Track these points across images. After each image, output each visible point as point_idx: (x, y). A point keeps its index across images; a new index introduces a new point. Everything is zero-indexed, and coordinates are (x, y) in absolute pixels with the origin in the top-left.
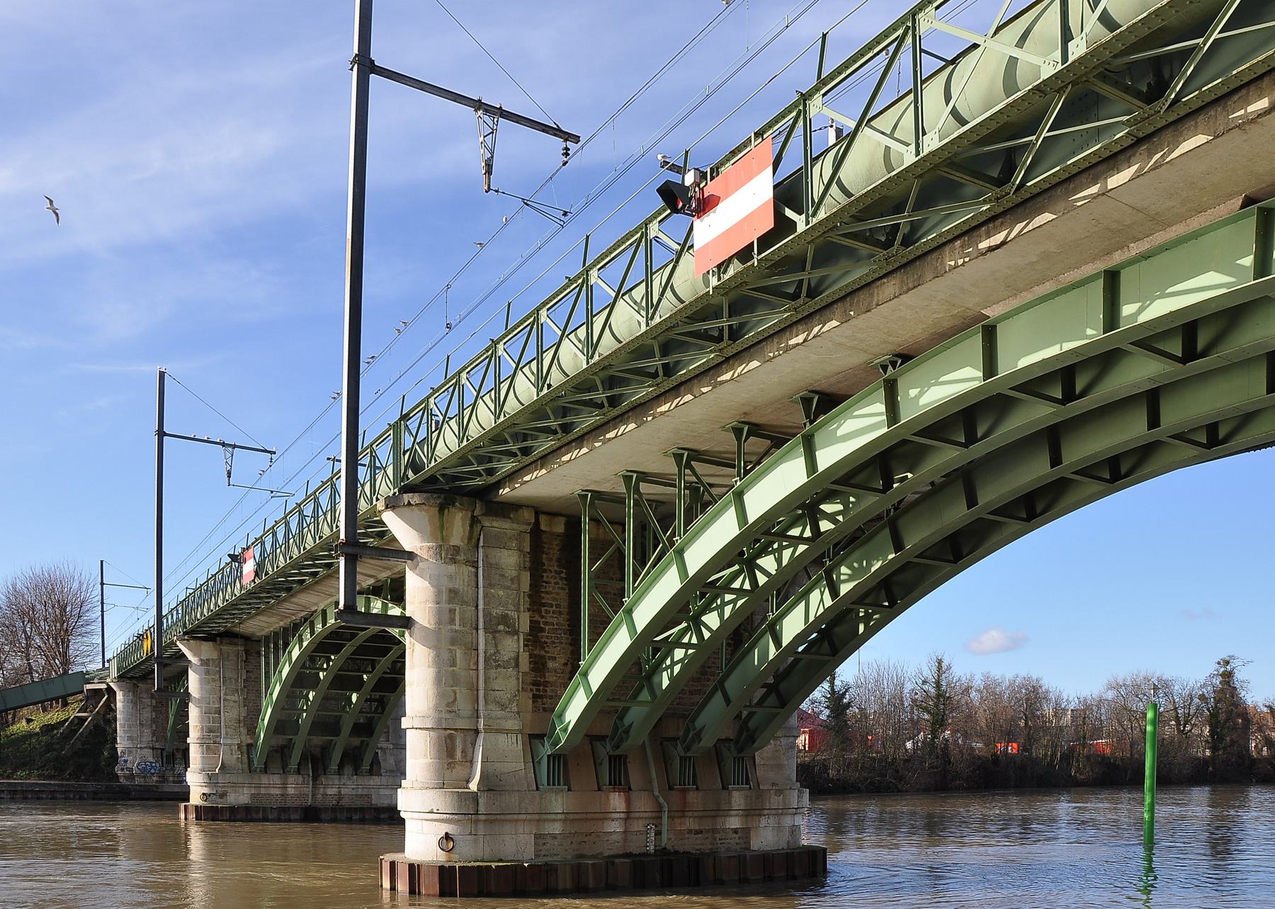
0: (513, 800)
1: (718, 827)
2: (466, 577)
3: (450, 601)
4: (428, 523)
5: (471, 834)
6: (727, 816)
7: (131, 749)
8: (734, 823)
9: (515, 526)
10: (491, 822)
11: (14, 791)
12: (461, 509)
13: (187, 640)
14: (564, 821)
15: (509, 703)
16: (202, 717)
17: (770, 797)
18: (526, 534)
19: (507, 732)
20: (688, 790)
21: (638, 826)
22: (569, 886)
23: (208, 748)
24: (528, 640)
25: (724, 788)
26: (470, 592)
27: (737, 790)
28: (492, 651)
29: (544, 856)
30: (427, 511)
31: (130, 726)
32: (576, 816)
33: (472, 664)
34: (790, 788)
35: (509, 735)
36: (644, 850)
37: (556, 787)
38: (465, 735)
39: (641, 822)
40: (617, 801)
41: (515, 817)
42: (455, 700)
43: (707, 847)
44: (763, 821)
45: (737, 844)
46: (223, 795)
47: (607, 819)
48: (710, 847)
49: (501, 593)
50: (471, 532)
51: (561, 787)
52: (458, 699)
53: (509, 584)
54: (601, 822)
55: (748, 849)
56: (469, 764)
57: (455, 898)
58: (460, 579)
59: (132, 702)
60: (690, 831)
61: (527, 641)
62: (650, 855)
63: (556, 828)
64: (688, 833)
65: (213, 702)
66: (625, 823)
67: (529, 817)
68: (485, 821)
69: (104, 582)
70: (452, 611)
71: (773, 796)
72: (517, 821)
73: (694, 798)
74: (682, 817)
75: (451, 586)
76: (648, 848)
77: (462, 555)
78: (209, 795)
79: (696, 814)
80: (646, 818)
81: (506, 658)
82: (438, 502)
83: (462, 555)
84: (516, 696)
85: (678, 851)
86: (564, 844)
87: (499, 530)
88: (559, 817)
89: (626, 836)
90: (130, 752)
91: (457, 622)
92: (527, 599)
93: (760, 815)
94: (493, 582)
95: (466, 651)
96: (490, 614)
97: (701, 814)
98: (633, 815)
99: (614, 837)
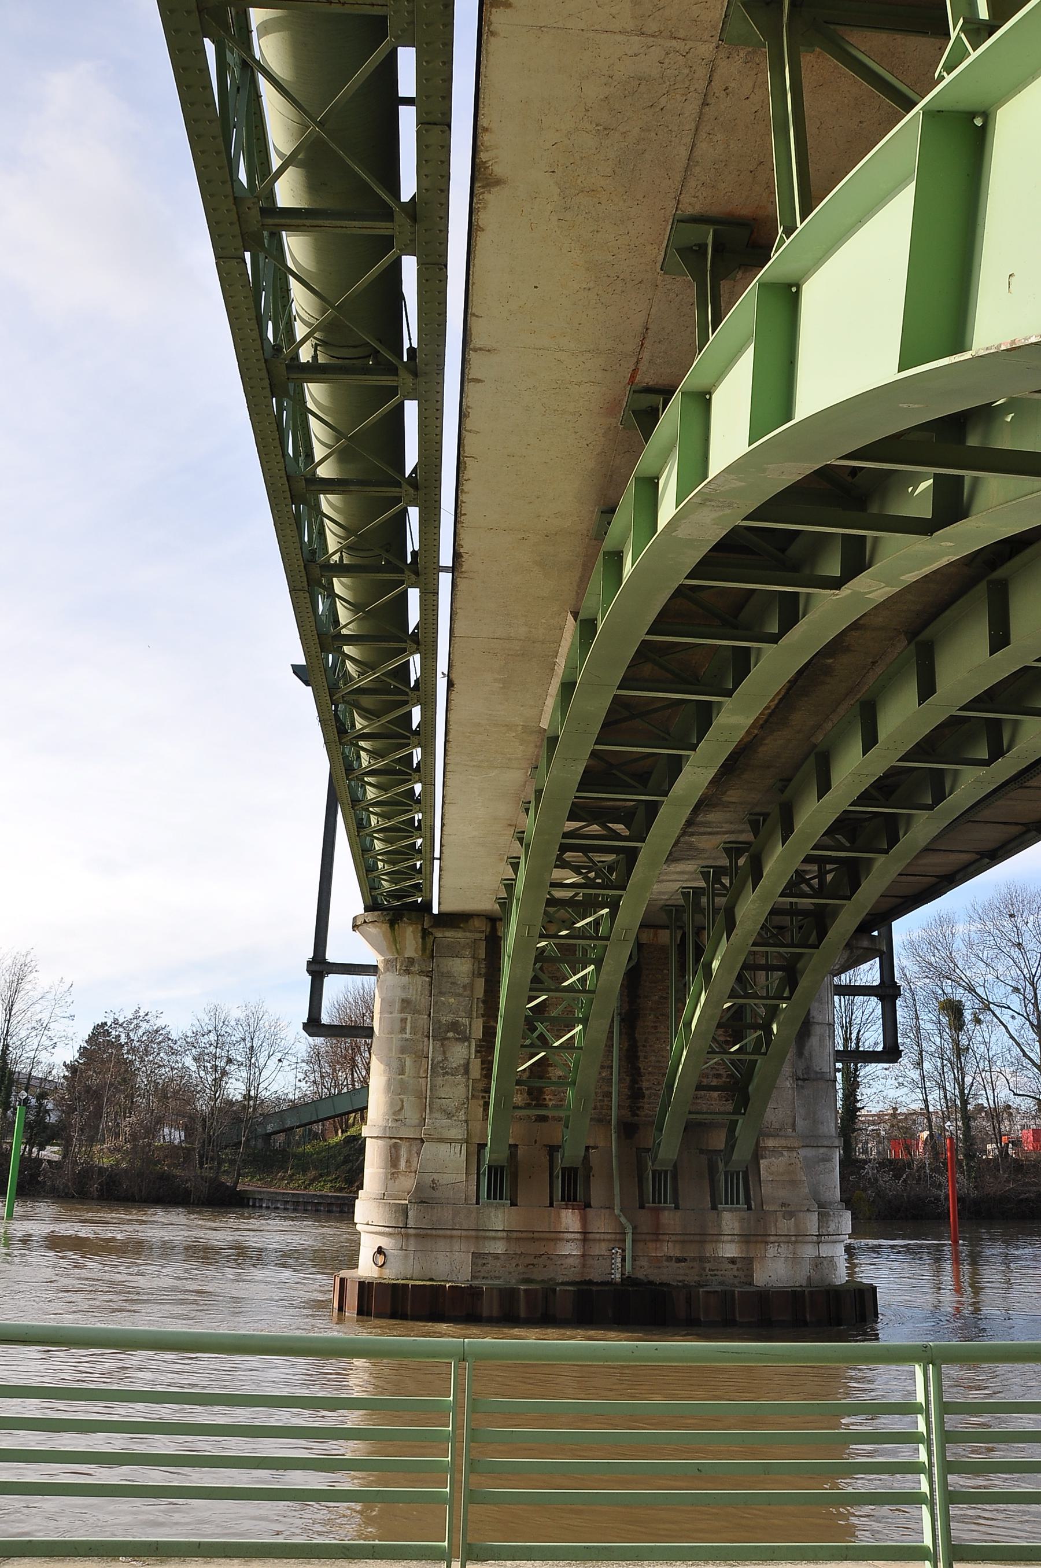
0: (446, 1214)
1: (708, 1255)
2: (420, 986)
3: (402, 1010)
4: (383, 939)
5: (401, 1249)
6: (717, 1241)
8: (730, 1250)
9: (468, 934)
10: (424, 1237)
11: (297, 1202)
12: (411, 924)
14: (508, 1239)
15: (457, 1111)
17: (777, 1221)
18: (482, 942)
19: (451, 1141)
20: (664, 1208)
21: (599, 1249)
22: (495, 1313)
24: (481, 1046)
25: (714, 1207)
26: (423, 1000)
27: (730, 1210)
28: (440, 1059)
29: (483, 1278)
30: (380, 928)
32: (519, 1235)
33: (421, 1071)
34: (808, 1210)
35: (453, 1144)
36: (607, 1278)
37: (498, 1201)
38: (411, 1145)
39: (604, 1246)
40: (570, 1220)
41: (448, 1232)
42: (402, 1108)
43: (692, 1278)
44: (771, 1251)
45: (735, 1277)
47: (561, 1240)
48: (697, 1278)
49: (452, 1000)
50: (424, 944)
51: (734, 1206)
52: (405, 1107)
53: (461, 991)
54: (553, 1243)
55: (751, 1284)
56: (413, 1174)
57: (369, 1318)
58: (413, 989)
60: (669, 1259)
61: (480, 1047)
62: (616, 1284)
63: (499, 1248)
64: (667, 1261)
66: (584, 1246)
67: (464, 1233)
68: (416, 1236)
69: (332, 956)
70: (404, 1020)
71: (780, 1219)
72: (452, 1237)
73: (670, 1219)
74: (657, 1241)
75: (404, 996)
76: (613, 1276)
77: (416, 966)
79: (673, 1238)
80: (609, 1240)
81: (454, 1065)
82: (387, 919)
83: (416, 966)
84: (464, 1104)
85: (653, 1282)
86: (508, 1265)
87: (452, 940)
88: (500, 1234)
89: (584, 1260)
91: (408, 1031)
92: (481, 1005)
93: (767, 1243)
94: (444, 990)
95: (416, 1059)
96: (439, 1022)
97: (679, 1238)
98: (591, 1236)
99: (570, 1261)
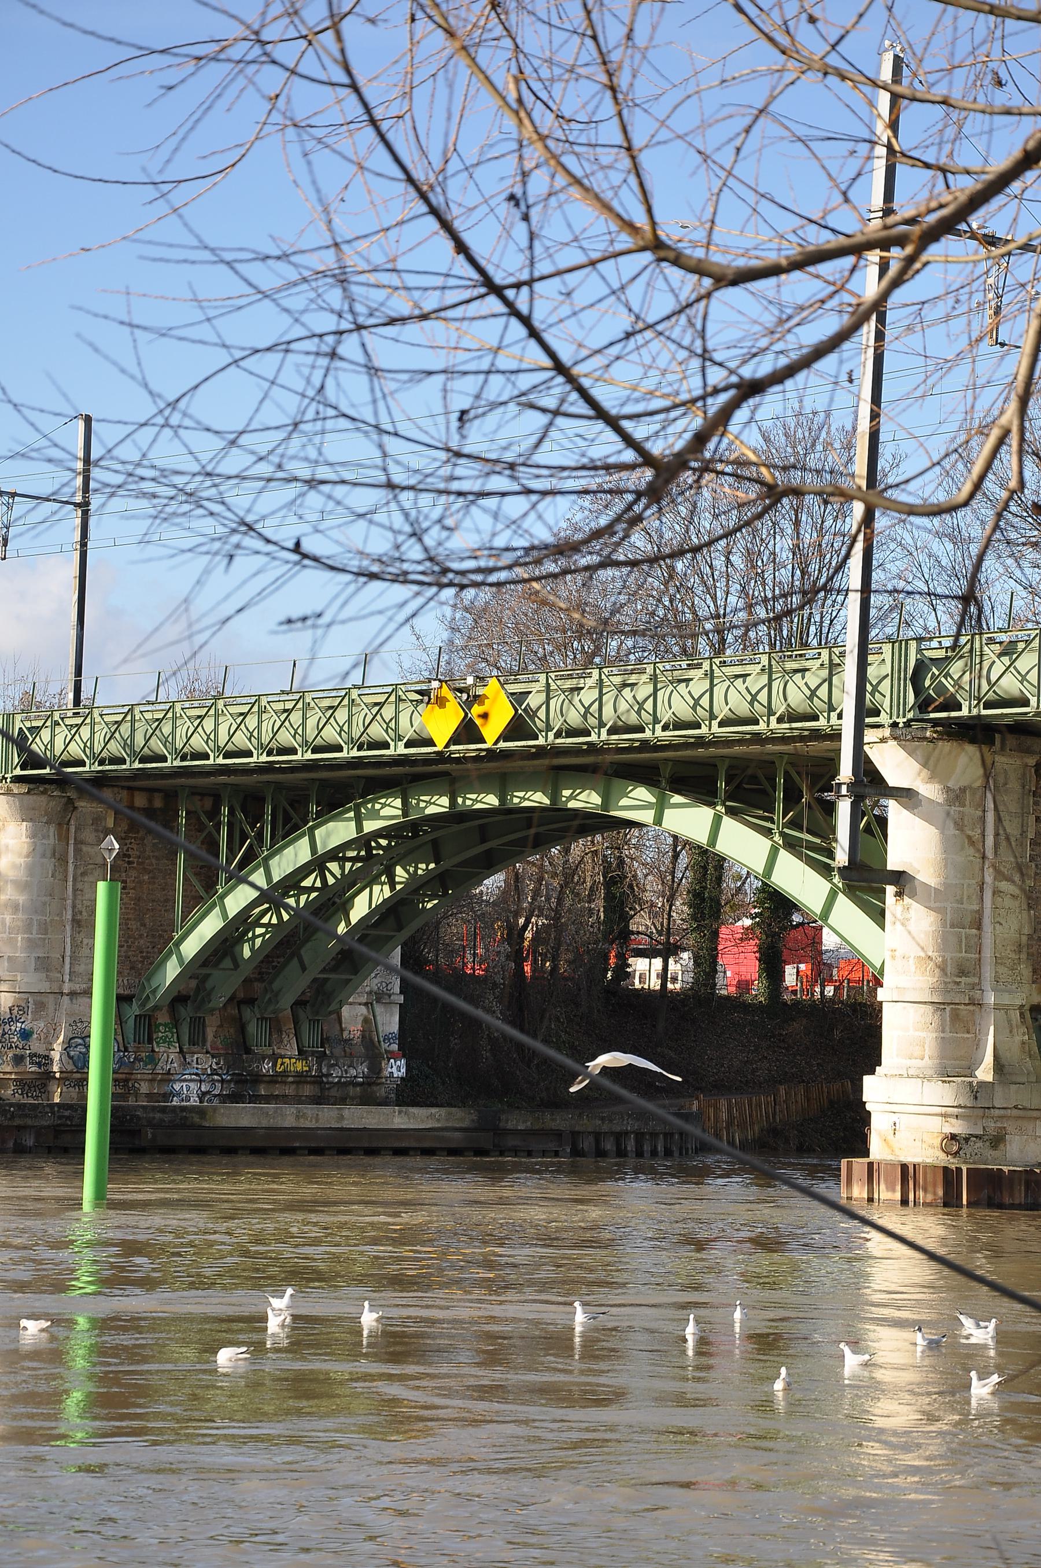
7: (43, 998)
13: (931, 740)
16: (944, 938)
23: (955, 1017)
31: (44, 928)
46: (997, 1141)
59: (54, 855)
65: (969, 897)
78: (967, 1140)
90: (41, 1006)
